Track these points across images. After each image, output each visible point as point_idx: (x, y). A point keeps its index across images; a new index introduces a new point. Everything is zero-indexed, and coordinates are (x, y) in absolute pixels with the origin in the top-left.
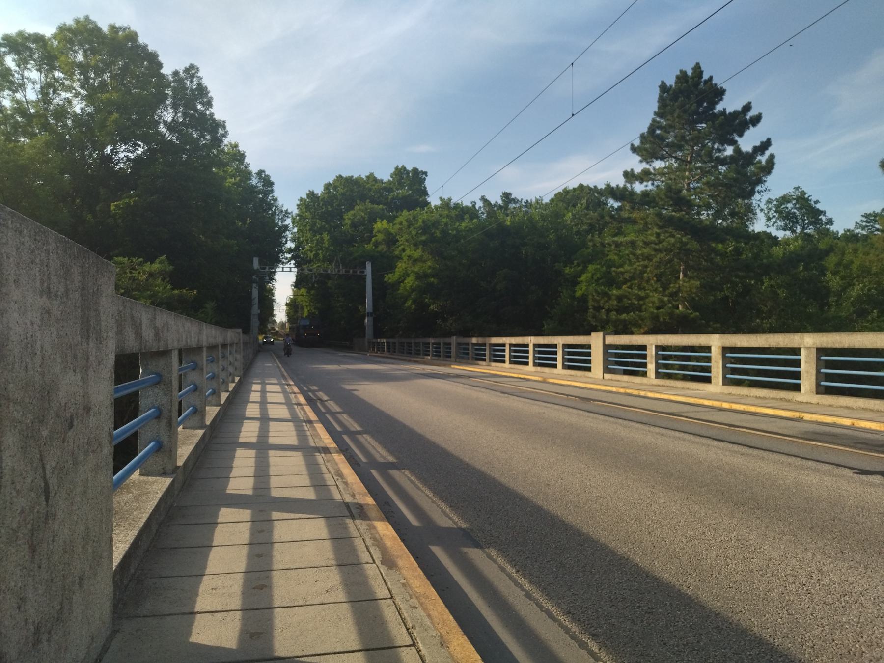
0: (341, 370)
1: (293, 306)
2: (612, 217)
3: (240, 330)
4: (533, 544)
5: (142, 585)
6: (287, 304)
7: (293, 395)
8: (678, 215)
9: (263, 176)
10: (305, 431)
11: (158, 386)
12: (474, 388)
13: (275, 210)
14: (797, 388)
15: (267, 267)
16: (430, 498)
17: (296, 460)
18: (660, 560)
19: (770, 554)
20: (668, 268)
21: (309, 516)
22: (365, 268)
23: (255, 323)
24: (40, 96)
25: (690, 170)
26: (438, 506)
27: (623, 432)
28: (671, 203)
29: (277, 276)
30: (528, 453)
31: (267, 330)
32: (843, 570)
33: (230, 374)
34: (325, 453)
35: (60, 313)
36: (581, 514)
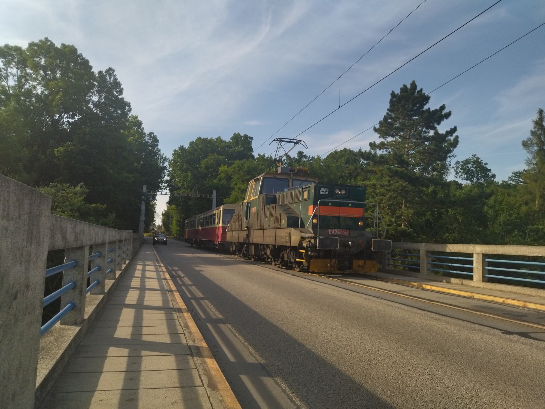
0: (194, 257)
1: (166, 216)
2: (362, 169)
3: (131, 231)
4: (304, 375)
5: (55, 397)
6: (163, 215)
7: (162, 273)
8: (401, 170)
9: (152, 136)
11: (75, 268)
12: (276, 271)
14: (471, 278)
16: (242, 343)
17: (160, 317)
20: (395, 201)
21: (165, 354)
22: (212, 193)
23: (142, 225)
24: (16, 83)
25: (408, 144)
26: (247, 348)
27: (365, 302)
28: (397, 162)
29: (158, 197)
31: (149, 230)
32: (491, 396)
33: (123, 259)
34: (179, 312)
35: (14, 229)
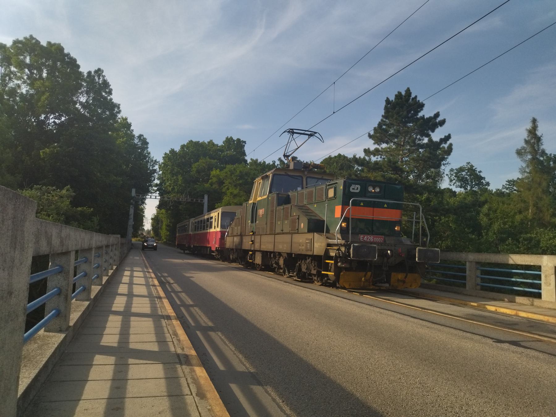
1: (156, 220)
3: (119, 236)
6: (152, 219)
7: (151, 279)
9: (142, 138)
10: (156, 304)
11: (60, 274)
13: (148, 159)
15: (141, 195)
16: (232, 351)
17: (148, 324)
18: (372, 396)
19: (439, 393)
21: (152, 362)
22: (203, 198)
23: (130, 230)
25: (403, 150)
26: (237, 357)
28: (391, 169)
29: (147, 201)
30: (297, 323)
32: (481, 404)
33: (111, 264)
34: (167, 319)
36: (326, 364)
